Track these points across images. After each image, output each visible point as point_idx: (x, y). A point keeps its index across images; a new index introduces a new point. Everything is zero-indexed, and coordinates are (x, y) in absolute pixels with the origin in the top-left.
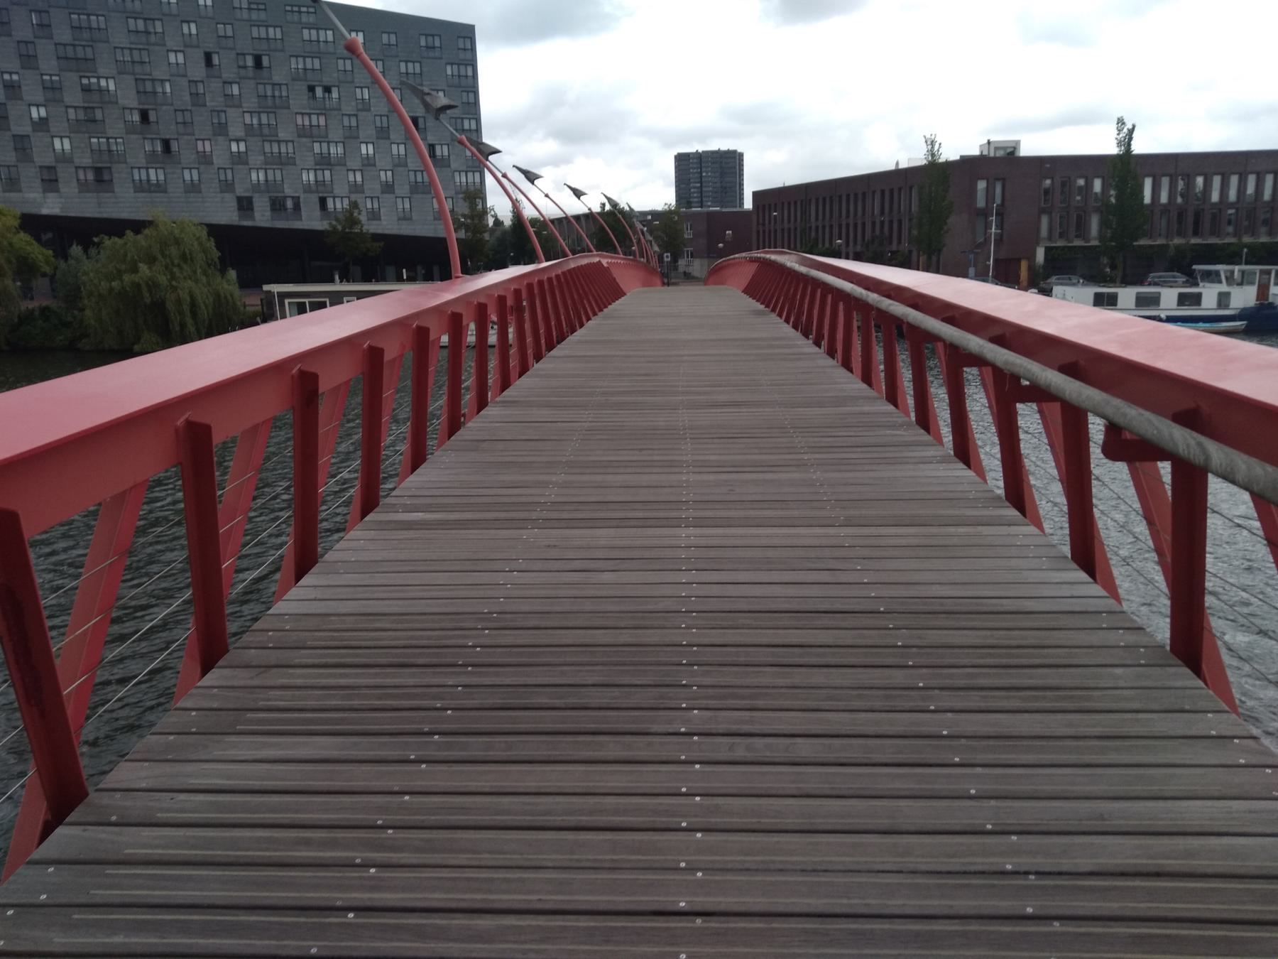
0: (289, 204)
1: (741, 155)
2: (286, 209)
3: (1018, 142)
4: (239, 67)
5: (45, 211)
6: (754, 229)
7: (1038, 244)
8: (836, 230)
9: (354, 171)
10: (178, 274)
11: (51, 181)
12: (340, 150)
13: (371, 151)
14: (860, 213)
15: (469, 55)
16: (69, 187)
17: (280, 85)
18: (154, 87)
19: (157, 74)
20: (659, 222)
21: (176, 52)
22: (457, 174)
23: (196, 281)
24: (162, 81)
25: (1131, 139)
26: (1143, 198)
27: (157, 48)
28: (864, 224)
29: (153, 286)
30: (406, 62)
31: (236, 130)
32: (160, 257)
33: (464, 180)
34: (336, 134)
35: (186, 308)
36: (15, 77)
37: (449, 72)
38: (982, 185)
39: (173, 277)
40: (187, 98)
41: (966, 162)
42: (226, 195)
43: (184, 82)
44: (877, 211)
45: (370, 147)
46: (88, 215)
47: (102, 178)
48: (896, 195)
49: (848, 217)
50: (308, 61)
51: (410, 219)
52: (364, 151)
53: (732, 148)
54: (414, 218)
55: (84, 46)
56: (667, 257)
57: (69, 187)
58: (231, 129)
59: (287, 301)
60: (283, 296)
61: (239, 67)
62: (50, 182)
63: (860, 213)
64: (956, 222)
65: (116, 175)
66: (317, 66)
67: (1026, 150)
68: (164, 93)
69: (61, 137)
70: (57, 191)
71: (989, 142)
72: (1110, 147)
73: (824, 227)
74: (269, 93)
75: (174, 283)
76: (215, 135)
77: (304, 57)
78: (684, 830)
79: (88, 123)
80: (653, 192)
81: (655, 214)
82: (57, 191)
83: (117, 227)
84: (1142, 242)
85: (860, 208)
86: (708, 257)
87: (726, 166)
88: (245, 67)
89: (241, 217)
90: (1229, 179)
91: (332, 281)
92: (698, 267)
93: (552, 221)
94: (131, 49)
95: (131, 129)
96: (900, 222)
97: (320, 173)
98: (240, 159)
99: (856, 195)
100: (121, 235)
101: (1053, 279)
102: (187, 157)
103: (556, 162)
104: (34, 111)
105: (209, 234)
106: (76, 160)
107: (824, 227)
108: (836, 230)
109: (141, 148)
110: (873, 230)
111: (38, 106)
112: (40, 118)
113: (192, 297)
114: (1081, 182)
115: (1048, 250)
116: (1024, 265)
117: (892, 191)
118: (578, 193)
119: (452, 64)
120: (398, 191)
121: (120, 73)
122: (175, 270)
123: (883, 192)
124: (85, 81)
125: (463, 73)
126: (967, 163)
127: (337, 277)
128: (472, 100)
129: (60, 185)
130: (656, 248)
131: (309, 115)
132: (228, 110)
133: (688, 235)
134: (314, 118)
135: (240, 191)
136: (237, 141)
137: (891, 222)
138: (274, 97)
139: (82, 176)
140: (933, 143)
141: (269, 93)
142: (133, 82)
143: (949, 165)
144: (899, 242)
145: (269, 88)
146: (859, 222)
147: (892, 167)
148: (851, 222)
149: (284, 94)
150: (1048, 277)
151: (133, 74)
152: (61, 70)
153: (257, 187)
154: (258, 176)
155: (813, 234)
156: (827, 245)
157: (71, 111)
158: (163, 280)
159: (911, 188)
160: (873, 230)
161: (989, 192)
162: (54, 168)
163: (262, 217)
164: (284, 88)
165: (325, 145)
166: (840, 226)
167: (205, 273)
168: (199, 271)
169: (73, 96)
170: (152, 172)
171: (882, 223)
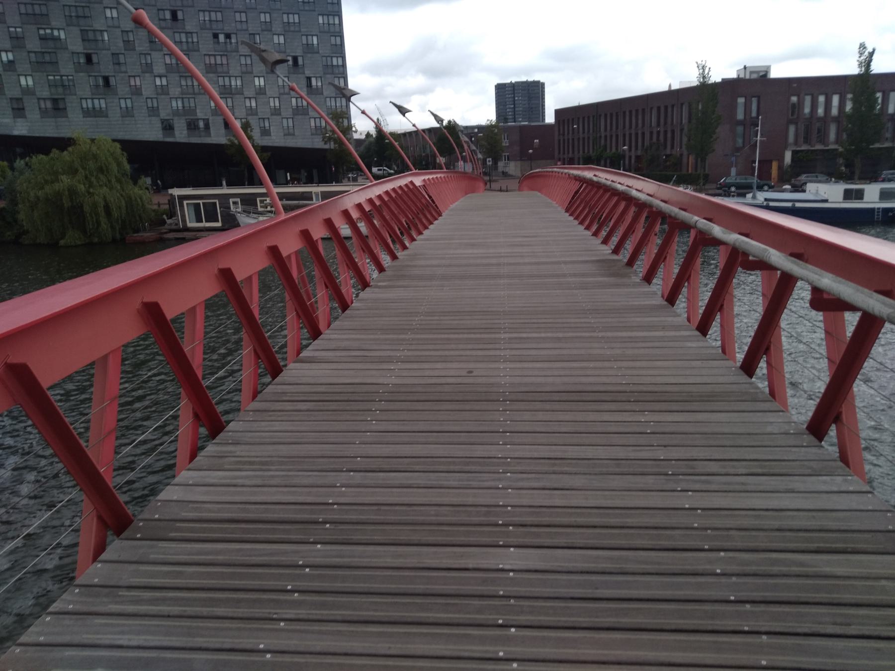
0: (201, 124)
1: (543, 84)
2: (199, 128)
3: (769, 67)
4: (160, 20)
5: (16, 133)
6: (556, 138)
7: (786, 148)
8: (621, 139)
9: (250, 98)
10: (95, 183)
11: (19, 109)
12: (239, 83)
13: (262, 83)
14: (640, 125)
15: (336, 9)
16: (33, 114)
17: (191, 33)
18: (95, 36)
19: (97, 26)
20: (484, 136)
21: (111, 8)
22: (328, 99)
23: (111, 189)
24: (102, 31)
25: (870, 61)
26: (736, 114)
27: (96, 5)
28: (643, 134)
29: (72, 192)
30: (288, 14)
31: (159, 69)
32: (80, 170)
33: (333, 104)
34: (235, 70)
35: (101, 210)
36: (18, 30)
37: (321, 21)
38: (741, 100)
39: (91, 185)
40: (121, 44)
41: (726, 83)
42: (153, 118)
43: (118, 32)
44: (654, 123)
45: (262, 80)
46: (48, 135)
47: (58, 108)
48: (670, 110)
49: (630, 127)
50: (213, 14)
51: (294, 135)
52: (257, 83)
53: (536, 79)
54: (296, 134)
55: (40, 5)
56: (489, 161)
57: (33, 114)
58: (155, 68)
59: (185, 202)
60: (182, 198)
61: (160, 20)
62: (19, 111)
63: (640, 125)
64: (722, 131)
65: (69, 105)
66: (219, 17)
67: (774, 74)
68: (103, 40)
69: (26, 76)
70: (24, 117)
71: (745, 68)
72: (850, 67)
73: (611, 136)
74: (184, 40)
75: (91, 190)
76: (143, 72)
77: (209, 11)
78: (501, 626)
79: (44, 63)
80: (477, 110)
81: (480, 128)
82: (24, 117)
83: (64, 143)
84: (877, 145)
85: (640, 122)
86: (521, 160)
87: (532, 92)
88: (165, 20)
89: (165, 136)
90: (889, 95)
91: (218, 185)
92: (513, 168)
93: (424, 131)
94: (76, 6)
95: (78, 68)
96: (673, 132)
97: (186, 100)
98: (163, 91)
99: (637, 111)
100: (47, 153)
101: (803, 177)
102: (122, 90)
103: (423, 91)
104: (4, 55)
105: (123, 150)
106: (37, 93)
107: (611, 136)
108: (621, 139)
109: (84, 84)
110: (651, 138)
111: (6, 51)
112: (9, 61)
113: (105, 201)
114: (794, 99)
115: (795, 153)
116: (775, 165)
117: (666, 107)
118: (403, 111)
119: (323, 15)
120: (284, 114)
121: (68, 25)
122: (93, 179)
123: (659, 108)
124: (42, 32)
125: (331, 22)
126: (727, 84)
127: (224, 183)
128: (338, 42)
129: (27, 113)
130: (480, 156)
131: (215, 55)
132: (153, 53)
133: (505, 143)
134: (218, 58)
135: (163, 114)
136: (160, 77)
137: (666, 132)
138: (187, 42)
139: (43, 106)
140: (704, 67)
141: (184, 40)
142: (79, 32)
143: (715, 85)
144: (672, 147)
145: (183, 35)
146: (640, 133)
147: (666, 89)
148: (633, 132)
149: (195, 40)
150: (798, 175)
151: (79, 26)
152: (22, 23)
153: (176, 113)
154: (177, 104)
155: (603, 141)
156: (614, 150)
157: (32, 55)
158: (82, 188)
159: (682, 104)
160: (651, 138)
161: (747, 106)
162: (21, 99)
163: (181, 135)
164: (195, 35)
165: (227, 79)
166: (624, 136)
167: (119, 181)
168: (113, 180)
169: (33, 44)
170: (96, 101)
171: (658, 132)
